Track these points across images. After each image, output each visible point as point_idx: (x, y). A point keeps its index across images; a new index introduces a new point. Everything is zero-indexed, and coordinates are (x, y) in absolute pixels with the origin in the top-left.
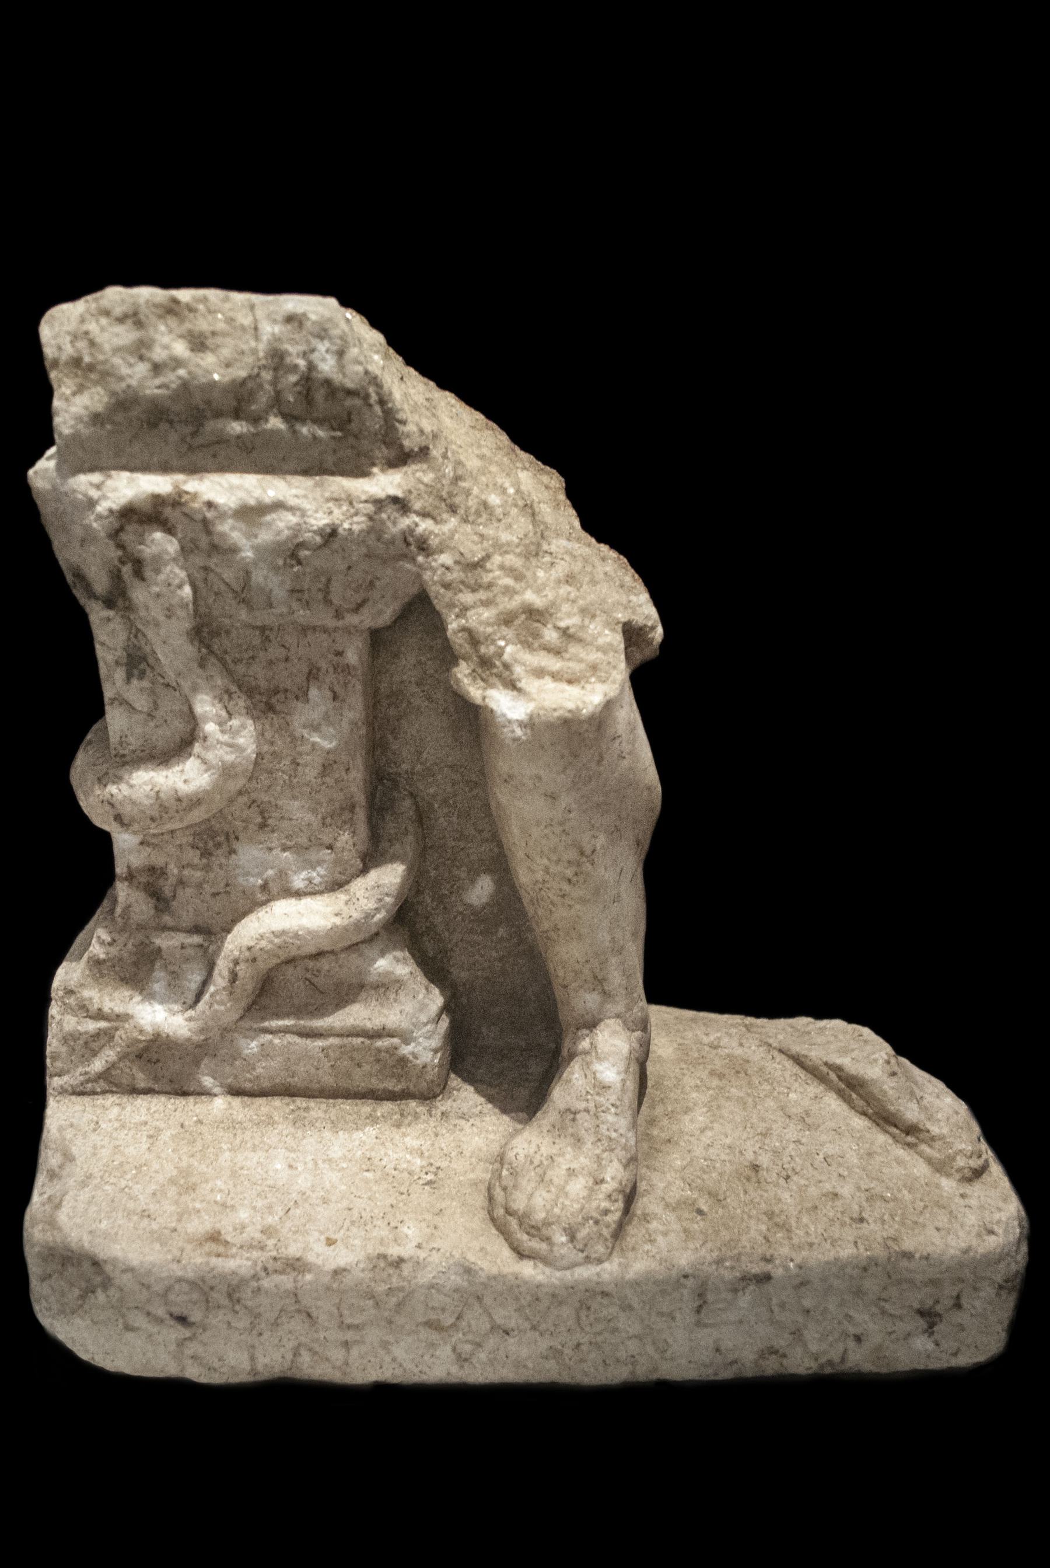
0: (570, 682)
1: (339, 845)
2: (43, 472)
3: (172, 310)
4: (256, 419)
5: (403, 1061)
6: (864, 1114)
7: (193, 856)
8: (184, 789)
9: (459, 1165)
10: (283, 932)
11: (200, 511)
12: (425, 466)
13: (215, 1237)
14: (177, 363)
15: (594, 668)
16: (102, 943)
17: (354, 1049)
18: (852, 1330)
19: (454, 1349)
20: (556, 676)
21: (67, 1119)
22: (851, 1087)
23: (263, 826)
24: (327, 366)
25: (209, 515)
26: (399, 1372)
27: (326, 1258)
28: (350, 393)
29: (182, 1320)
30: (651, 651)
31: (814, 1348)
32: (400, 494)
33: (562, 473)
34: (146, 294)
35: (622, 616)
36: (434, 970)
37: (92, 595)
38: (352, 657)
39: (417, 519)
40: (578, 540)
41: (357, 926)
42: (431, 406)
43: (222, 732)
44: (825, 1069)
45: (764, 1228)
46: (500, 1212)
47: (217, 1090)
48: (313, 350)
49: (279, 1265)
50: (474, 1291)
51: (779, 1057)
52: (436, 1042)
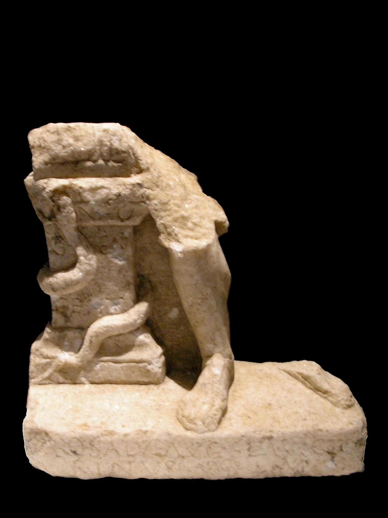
0: (196, 239)
1: (125, 297)
2: (29, 179)
3: (69, 129)
4: (95, 161)
5: (148, 371)
6: (310, 388)
7: (77, 302)
8: (74, 278)
9: (167, 404)
10: (107, 326)
11: (78, 190)
12: (148, 173)
13: (85, 425)
14: (70, 145)
15: (204, 235)
16: (48, 333)
17: (132, 367)
18: (305, 459)
19: (166, 464)
20: (191, 237)
21: (35, 393)
22: (305, 379)
23: (100, 291)
24: (116, 144)
25: (80, 191)
26: (148, 473)
27: (120, 430)
28: (124, 152)
29: (75, 452)
30: (225, 231)
31: (292, 465)
32: (140, 182)
33: (196, 175)
34: (61, 125)
35: (214, 218)
36: (159, 341)
37: (44, 217)
38: (126, 234)
39: (146, 189)
40: (200, 195)
41: (131, 324)
42: (151, 155)
43: (86, 260)
44: (297, 375)
45: (270, 422)
46: (180, 417)
47: (86, 382)
48: (111, 140)
49: (106, 433)
50: (172, 442)
51: (282, 372)
52: (160, 364)
